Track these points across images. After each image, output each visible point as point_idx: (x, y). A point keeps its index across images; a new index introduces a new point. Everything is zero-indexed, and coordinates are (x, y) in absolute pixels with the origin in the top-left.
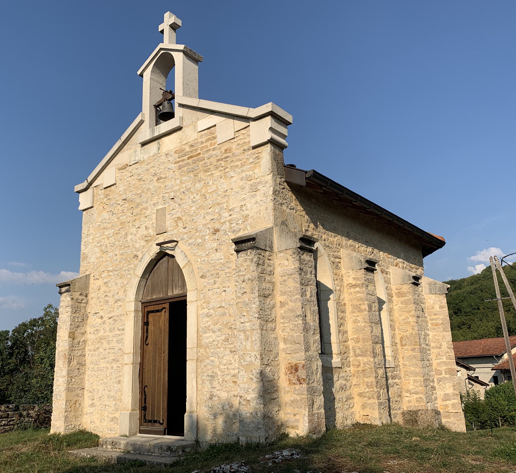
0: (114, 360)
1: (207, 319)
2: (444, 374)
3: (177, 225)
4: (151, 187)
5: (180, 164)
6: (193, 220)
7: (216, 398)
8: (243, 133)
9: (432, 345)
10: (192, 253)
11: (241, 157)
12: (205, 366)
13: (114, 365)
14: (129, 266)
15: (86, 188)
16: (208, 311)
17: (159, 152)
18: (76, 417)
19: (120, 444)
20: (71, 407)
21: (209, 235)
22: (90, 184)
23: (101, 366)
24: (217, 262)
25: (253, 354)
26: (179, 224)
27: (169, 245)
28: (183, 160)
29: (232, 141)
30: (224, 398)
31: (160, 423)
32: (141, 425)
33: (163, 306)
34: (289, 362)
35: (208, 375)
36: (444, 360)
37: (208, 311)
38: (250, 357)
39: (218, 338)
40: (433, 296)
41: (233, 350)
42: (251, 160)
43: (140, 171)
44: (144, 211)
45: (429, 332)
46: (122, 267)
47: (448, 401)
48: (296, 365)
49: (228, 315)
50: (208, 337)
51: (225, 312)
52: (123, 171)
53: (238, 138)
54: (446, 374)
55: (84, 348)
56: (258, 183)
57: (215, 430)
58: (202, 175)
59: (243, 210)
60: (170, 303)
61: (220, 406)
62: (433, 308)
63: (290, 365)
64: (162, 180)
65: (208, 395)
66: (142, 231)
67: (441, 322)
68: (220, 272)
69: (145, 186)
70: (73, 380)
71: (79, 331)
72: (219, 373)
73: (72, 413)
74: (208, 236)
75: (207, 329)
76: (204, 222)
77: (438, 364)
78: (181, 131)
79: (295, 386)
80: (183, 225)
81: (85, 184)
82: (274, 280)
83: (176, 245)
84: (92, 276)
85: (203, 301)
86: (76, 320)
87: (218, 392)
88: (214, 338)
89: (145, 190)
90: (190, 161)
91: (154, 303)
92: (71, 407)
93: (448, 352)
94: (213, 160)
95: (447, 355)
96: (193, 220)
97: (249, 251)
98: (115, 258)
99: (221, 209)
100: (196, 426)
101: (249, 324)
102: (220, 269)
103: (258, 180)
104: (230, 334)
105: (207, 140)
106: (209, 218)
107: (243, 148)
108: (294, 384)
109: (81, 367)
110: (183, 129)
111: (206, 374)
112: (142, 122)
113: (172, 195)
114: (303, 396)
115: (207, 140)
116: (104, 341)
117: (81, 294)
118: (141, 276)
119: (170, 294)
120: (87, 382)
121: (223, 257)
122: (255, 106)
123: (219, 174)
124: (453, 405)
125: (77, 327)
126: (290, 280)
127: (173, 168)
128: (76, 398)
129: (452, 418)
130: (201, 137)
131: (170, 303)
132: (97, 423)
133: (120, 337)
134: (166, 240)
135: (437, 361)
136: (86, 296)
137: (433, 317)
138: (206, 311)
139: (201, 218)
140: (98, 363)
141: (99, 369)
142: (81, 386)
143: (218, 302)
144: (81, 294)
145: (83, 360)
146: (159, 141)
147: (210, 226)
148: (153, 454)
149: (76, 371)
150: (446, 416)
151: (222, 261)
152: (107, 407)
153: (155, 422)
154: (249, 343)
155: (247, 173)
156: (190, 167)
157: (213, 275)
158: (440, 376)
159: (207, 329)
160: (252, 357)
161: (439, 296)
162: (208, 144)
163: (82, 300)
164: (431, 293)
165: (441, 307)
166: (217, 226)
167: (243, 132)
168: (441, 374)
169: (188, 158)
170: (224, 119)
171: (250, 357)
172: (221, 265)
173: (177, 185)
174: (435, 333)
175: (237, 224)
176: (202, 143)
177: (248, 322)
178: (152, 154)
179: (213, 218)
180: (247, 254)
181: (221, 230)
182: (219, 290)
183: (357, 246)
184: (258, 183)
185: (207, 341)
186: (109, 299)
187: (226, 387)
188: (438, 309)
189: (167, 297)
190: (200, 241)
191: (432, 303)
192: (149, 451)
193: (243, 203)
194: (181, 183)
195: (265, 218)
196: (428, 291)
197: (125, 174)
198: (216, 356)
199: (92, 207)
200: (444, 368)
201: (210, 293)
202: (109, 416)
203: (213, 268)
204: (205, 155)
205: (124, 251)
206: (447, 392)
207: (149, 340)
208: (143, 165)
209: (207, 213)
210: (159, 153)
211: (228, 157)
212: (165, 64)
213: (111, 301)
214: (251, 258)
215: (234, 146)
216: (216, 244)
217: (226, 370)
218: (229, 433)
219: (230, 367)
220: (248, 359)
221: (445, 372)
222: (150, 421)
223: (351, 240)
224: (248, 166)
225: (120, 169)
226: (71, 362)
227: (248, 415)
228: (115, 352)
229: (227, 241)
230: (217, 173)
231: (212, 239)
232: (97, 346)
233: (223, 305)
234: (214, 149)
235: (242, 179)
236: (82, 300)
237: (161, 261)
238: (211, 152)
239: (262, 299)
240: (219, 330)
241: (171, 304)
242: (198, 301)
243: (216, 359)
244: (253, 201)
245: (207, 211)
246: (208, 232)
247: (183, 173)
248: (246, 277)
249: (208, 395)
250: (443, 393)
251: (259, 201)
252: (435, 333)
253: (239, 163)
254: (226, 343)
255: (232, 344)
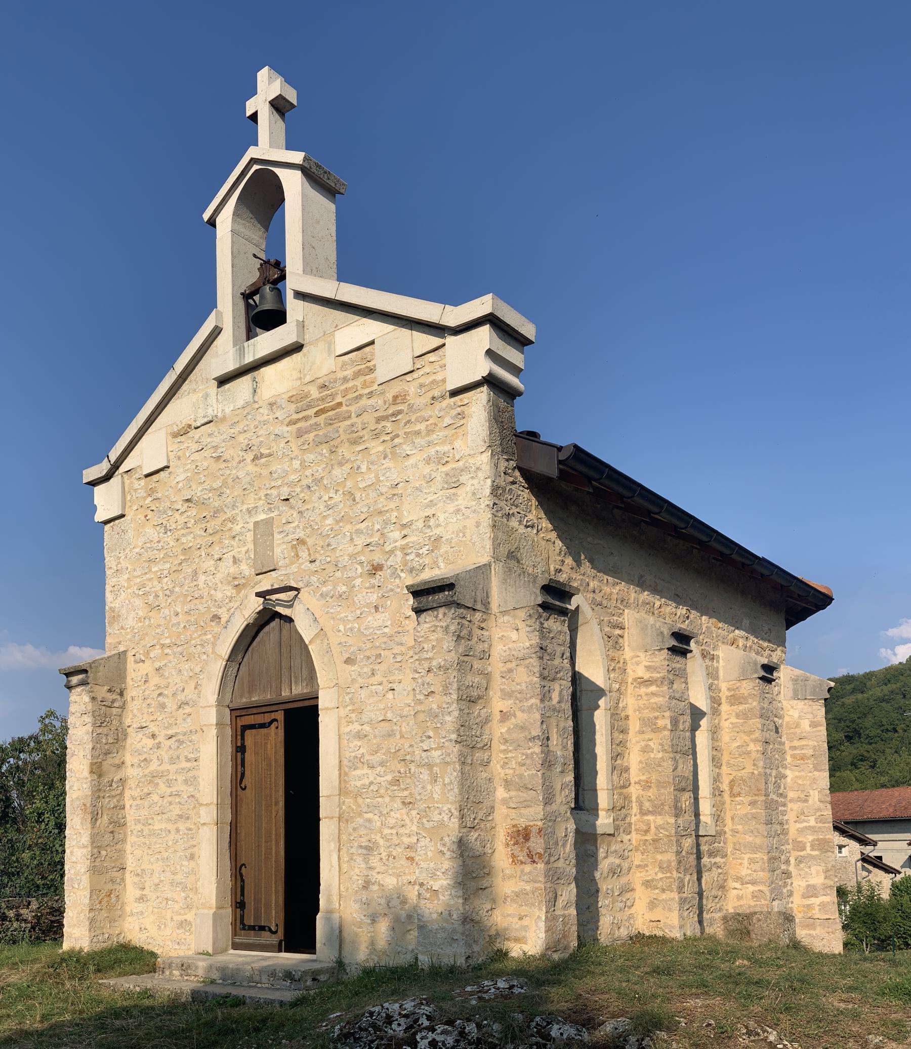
0: (180, 816)
1: (359, 743)
2: (808, 848)
3: (298, 556)
4: (241, 474)
5: (299, 425)
6: (329, 545)
7: (375, 888)
8: (432, 359)
9: (791, 795)
10: (327, 613)
11: (426, 414)
12: (354, 829)
13: (182, 826)
14: (204, 638)
15: (107, 474)
16: (360, 728)
17: (256, 398)
18: (112, 921)
19: (197, 967)
20: (100, 902)
21: (361, 576)
22: (115, 467)
23: (155, 828)
24: (378, 632)
25: (445, 809)
26: (301, 554)
27: (282, 596)
28: (306, 418)
29: (408, 377)
30: (391, 887)
31: (270, 930)
32: (235, 934)
33: (273, 716)
34: (514, 822)
35: (361, 847)
36: (812, 822)
37: (360, 728)
38: (440, 814)
39: (378, 778)
40: (800, 704)
41: (408, 800)
42: (447, 421)
43: (217, 440)
44: (230, 525)
45: (788, 772)
46: (189, 637)
47: (812, 899)
48: (526, 828)
49: (398, 736)
50: (361, 777)
51: (392, 731)
52: (182, 439)
53: (421, 372)
54: (812, 849)
55: (122, 794)
56: (462, 471)
57: (372, 943)
58: (345, 451)
59: (429, 527)
60: (286, 711)
61: (383, 901)
62: (798, 726)
63: (515, 829)
64: (263, 460)
65: (360, 882)
66: (227, 567)
67: (811, 752)
68: (382, 652)
69: (228, 472)
70: (104, 853)
71: (109, 761)
72: (382, 842)
73: (104, 914)
74: (360, 580)
75: (358, 762)
76: (351, 549)
77: (801, 831)
78: (301, 354)
79: (523, 866)
80: (310, 554)
81: (103, 468)
82: (490, 669)
83: (296, 596)
84: (130, 654)
85: (349, 708)
86: (104, 741)
87: (380, 877)
88: (371, 779)
89: (230, 481)
90: (321, 419)
91: (255, 711)
92: (100, 902)
93: (819, 809)
94: (369, 418)
95: (818, 814)
96: (329, 545)
97: (442, 611)
98: (175, 620)
99: (386, 523)
100: (339, 937)
101: (438, 753)
102: (383, 646)
103: (460, 463)
104: (402, 770)
105: (357, 375)
106: (360, 541)
107: (430, 395)
108: (522, 863)
109: (117, 829)
110: (305, 350)
111: (356, 844)
112: (216, 332)
113: (285, 492)
114: (537, 885)
115: (357, 375)
116: (159, 781)
117: (110, 691)
118: (227, 657)
119: (285, 693)
120: (130, 856)
121: (389, 623)
122: (456, 302)
123: (381, 448)
124: (823, 906)
125: (106, 754)
126: (521, 669)
127: (286, 435)
128: (110, 886)
129: (818, 928)
130: (343, 366)
131: (286, 711)
132: (153, 931)
133: (190, 774)
134: (276, 586)
135: (798, 825)
136: (121, 694)
137: (796, 743)
138: (356, 727)
139: (345, 541)
140: (150, 821)
141: (152, 834)
142: (118, 864)
143: (380, 710)
144: (110, 691)
145: (120, 816)
146: (255, 374)
147: (363, 558)
148: (259, 985)
149: (108, 838)
150: (808, 926)
151: (386, 630)
152: (170, 902)
153: (262, 928)
154: (437, 789)
155: (438, 448)
156: (321, 433)
157: (368, 658)
158: (802, 853)
159: (358, 762)
160: (443, 814)
161: (811, 703)
162: (358, 383)
163: (113, 701)
164: (795, 697)
165: (813, 725)
166: (378, 558)
167: (432, 357)
168: (804, 849)
169: (317, 414)
170: (391, 327)
171: (440, 814)
172: (385, 639)
173: (296, 470)
174: (797, 774)
175: (418, 555)
176: (345, 380)
177: (436, 749)
178: (240, 403)
179: (369, 541)
180: (436, 617)
181: (385, 568)
182: (381, 688)
183: (658, 604)
184: (462, 471)
185: (359, 784)
186: (166, 701)
187: (394, 868)
188: (808, 728)
189: (280, 700)
190: (344, 588)
191: (796, 715)
192: (250, 979)
193: (429, 512)
194: (304, 466)
195: (474, 544)
196: (791, 694)
197: (186, 445)
198: (376, 812)
199: (122, 516)
200: (810, 838)
201: (364, 694)
202: (175, 918)
203: (369, 645)
204: (353, 408)
205: (193, 607)
206: (812, 882)
207: (247, 781)
208: (224, 428)
209: (358, 532)
210: (255, 402)
211: (400, 412)
212: (263, 198)
213: (171, 705)
214: (444, 624)
215: (412, 389)
216: (375, 596)
217: (395, 837)
218: (400, 949)
219: (401, 831)
220: (436, 818)
221: (812, 846)
222: (252, 928)
223: (646, 593)
224: (441, 434)
225: (175, 435)
226: (96, 820)
227: (435, 916)
228: (183, 801)
229: (399, 590)
230: (377, 447)
231: (367, 585)
232: (146, 791)
233: (389, 716)
234: (371, 395)
235: (428, 461)
236: (113, 701)
237: (266, 629)
238: (364, 402)
239: (464, 705)
240: (382, 764)
241: (287, 712)
242: (341, 709)
243: (376, 818)
244: (451, 508)
245: (358, 527)
246: (360, 570)
247: (306, 447)
248: (434, 663)
249: (360, 882)
250: (804, 884)
251: (462, 507)
252: (797, 774)
253: (421, 427)
254: (395, 788)
255: (406, 789)
